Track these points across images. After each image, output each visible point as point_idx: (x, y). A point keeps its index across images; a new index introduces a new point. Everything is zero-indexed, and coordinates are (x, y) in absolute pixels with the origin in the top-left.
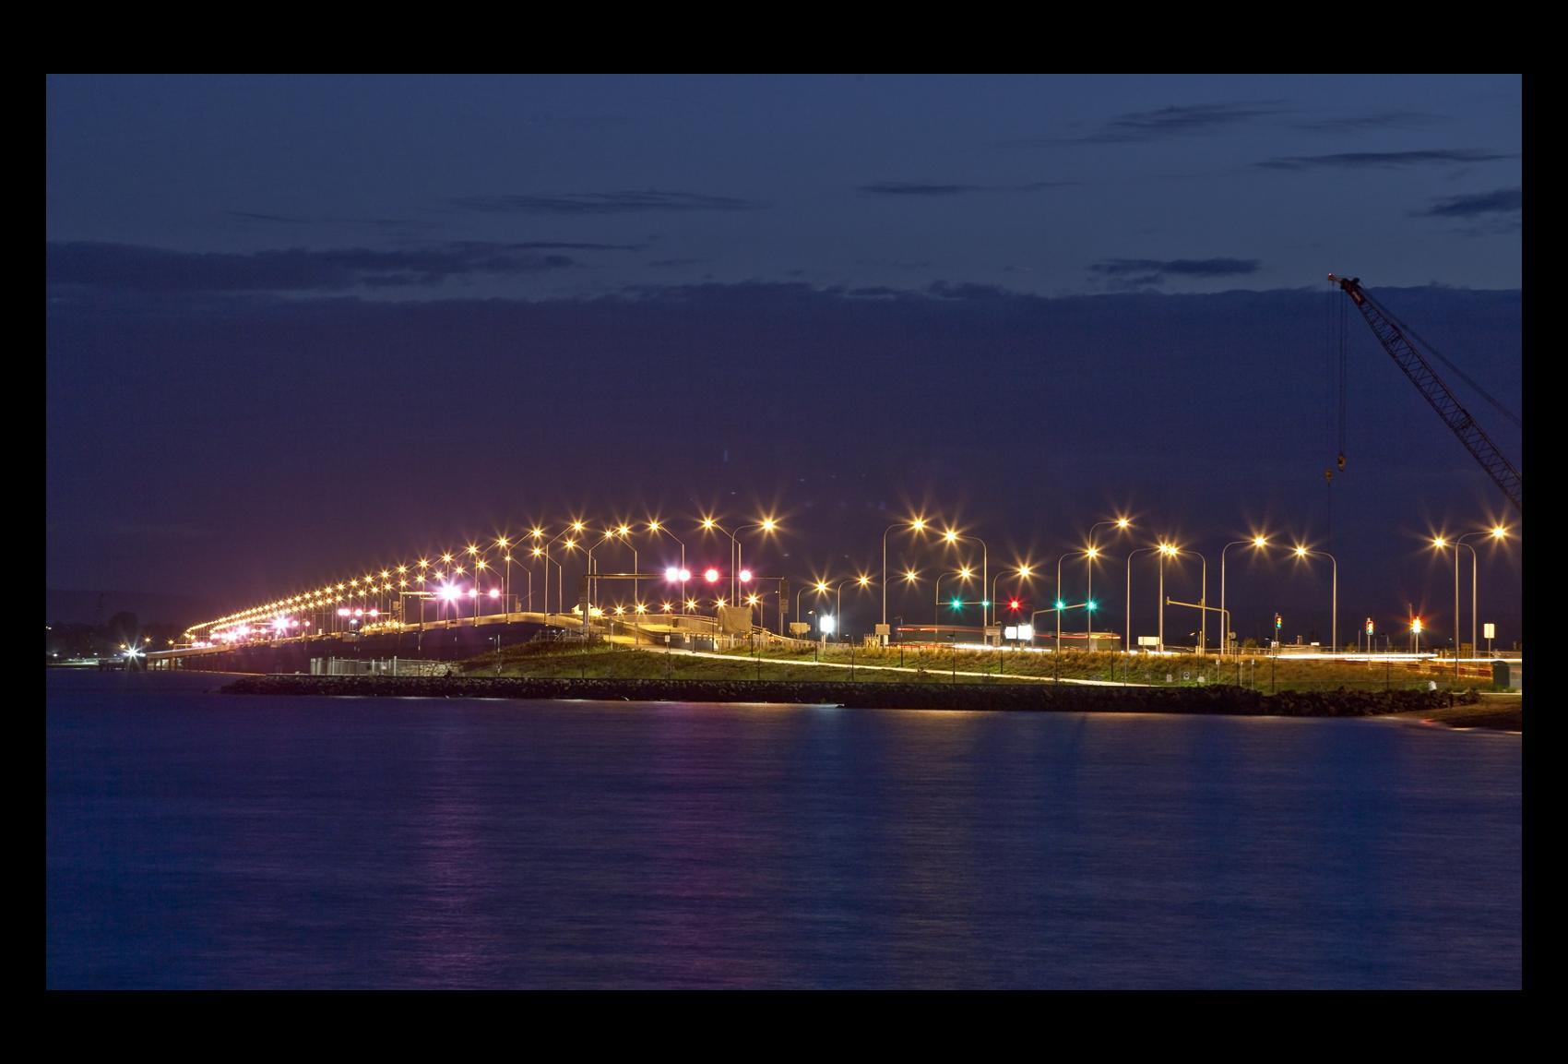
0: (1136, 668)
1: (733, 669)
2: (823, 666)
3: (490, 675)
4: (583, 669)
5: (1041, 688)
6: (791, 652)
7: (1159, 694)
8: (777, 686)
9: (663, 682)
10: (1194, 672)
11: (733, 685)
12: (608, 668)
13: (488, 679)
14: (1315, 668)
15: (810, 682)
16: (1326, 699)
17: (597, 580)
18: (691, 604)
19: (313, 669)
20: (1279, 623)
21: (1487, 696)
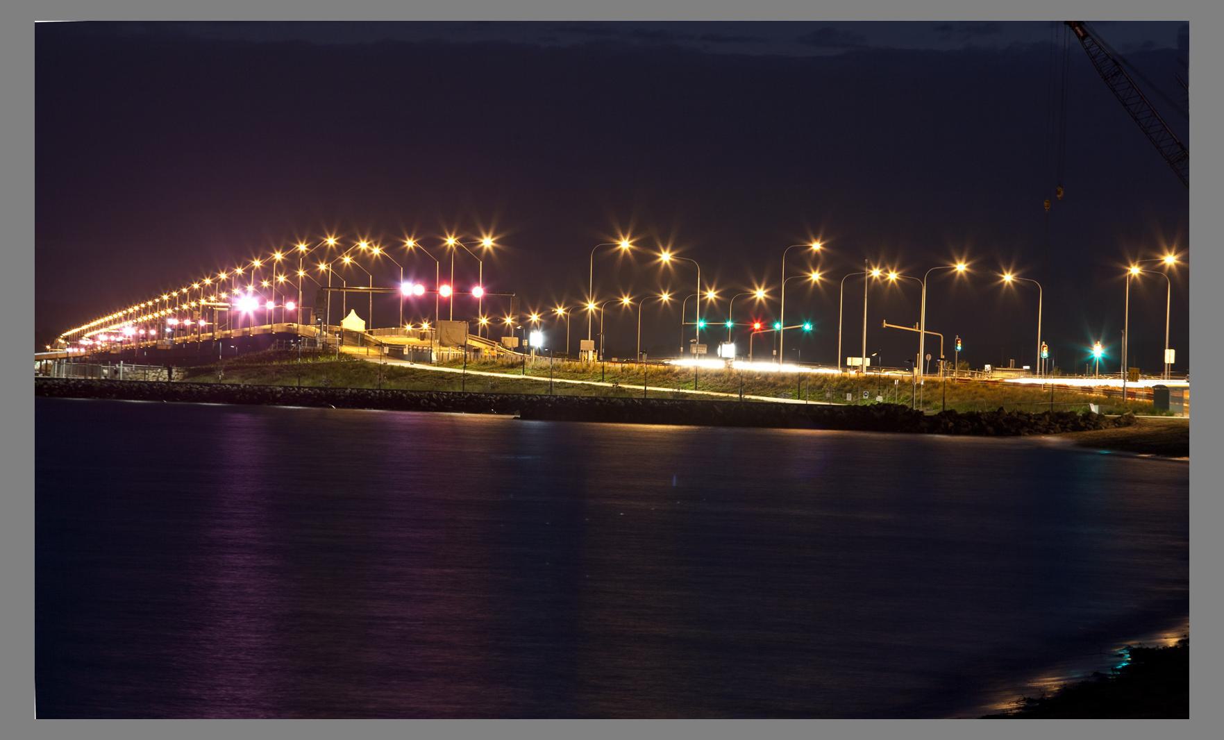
0: (822, 387)
1: (441, 380)
2: (527, 379)
3: (212, 382)
4: (299, 377)
5: (729, 403)
6: (502, 366)
7: (826, 412)
8: (476, 397)
9: (369, 392)
10: (876, 391)
11: (434, 396)
12: (324, 377)
13: (207, 385)
14: (990, 390)
15: (507, 395)
16: (985, 420)
17: (346, 292)
18: (484, 321)
19: (52, 373)
20: (959, 347)
21: (1142, 419)
